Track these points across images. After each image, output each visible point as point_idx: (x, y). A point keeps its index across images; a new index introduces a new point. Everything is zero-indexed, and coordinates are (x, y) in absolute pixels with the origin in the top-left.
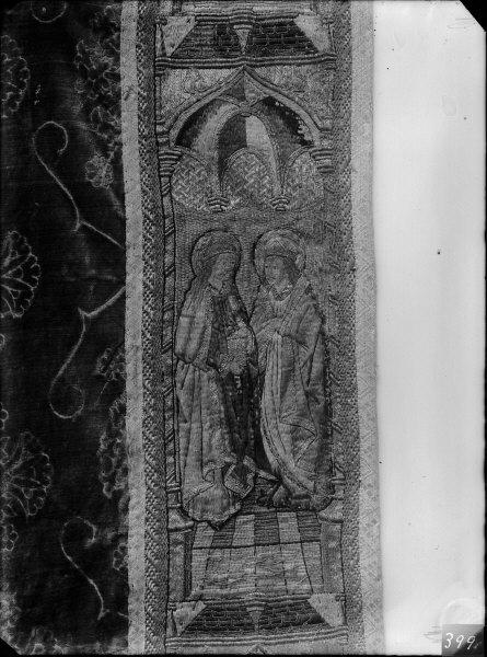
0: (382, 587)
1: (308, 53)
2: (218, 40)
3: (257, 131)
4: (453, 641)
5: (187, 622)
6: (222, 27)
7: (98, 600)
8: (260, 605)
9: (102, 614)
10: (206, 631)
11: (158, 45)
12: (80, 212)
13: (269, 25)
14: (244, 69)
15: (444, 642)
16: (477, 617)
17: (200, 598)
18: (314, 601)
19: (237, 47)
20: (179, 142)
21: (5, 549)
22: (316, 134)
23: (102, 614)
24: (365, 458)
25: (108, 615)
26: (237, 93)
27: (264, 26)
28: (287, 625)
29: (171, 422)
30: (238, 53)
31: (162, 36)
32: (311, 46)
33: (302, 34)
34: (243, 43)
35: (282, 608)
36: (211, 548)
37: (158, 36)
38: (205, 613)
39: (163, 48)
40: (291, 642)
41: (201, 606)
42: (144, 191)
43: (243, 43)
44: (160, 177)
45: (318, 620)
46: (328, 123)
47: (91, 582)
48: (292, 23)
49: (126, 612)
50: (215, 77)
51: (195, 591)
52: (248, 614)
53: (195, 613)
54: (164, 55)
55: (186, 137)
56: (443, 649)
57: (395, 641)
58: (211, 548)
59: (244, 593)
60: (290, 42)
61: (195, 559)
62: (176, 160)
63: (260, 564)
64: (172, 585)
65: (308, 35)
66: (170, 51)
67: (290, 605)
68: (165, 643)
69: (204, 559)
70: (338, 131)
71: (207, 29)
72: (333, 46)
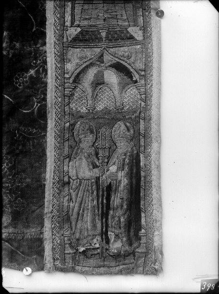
3: (112, 77)
4: (206, 286)
5: (73, 36)
7: (33, 23)
8: (106, 30)
9: (34, 29)
10: (81, 41)
12: (27, 113)
14: (105, 48)
15: (202, 286)
16: (217, 277)
17: (79, 26)
18: (129, 29)
19: (100, 39)
20: (74, 81)
23: (34, 29)
24: (155, 90)
25: (37, 30)
26: (101, 58)
28: (117, 40)
35: (116, 32)
36: (83, 4)
38: (81, 33)
40: (119, 47)
41: (79, 30)
45: (131, 38)
47: (30, 15)
49: (45, 29)
50: (90, 53)
51: (77, 23)
52: (100, 33)
53: (76, 33)
55: (77, 79)
56: (201, 290)
58: (83, 4)
59: (99, 24)
61: (76, 8)
62: (73, 89)
63: (106, 12)
64: (66, 19)
67: (119, 31)
69: (80, 8)
70: (146, 72)
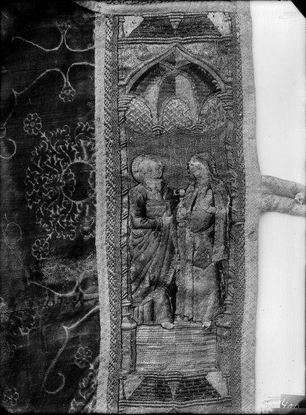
0: (255, 350)
1: (214, 397)
2: (156, 28)
6: (161, 382)
11: (121, 392)
13: (190, 381)
16: (303, 393)
21: (2, 106)
22: (222, 85)
27: (187, 382)
29: (126, 221)
30: (170, 399)
31: (123, 386)
32: (216, 392)
33: (210, 385)
34: (174, 393)
37: (121, 387)
39: (124, 394)
42: (106, 139)
43: (174, 393)
44: (122, 317)
46: (230, 79)
48: (205, 379)
54: (124, 398)
57: (261, 407)
60: (203, 391)
65: (214, 386)
66: (128, 395)
68: (121, 303)
71: (150, 383)
72: (233, 29)
